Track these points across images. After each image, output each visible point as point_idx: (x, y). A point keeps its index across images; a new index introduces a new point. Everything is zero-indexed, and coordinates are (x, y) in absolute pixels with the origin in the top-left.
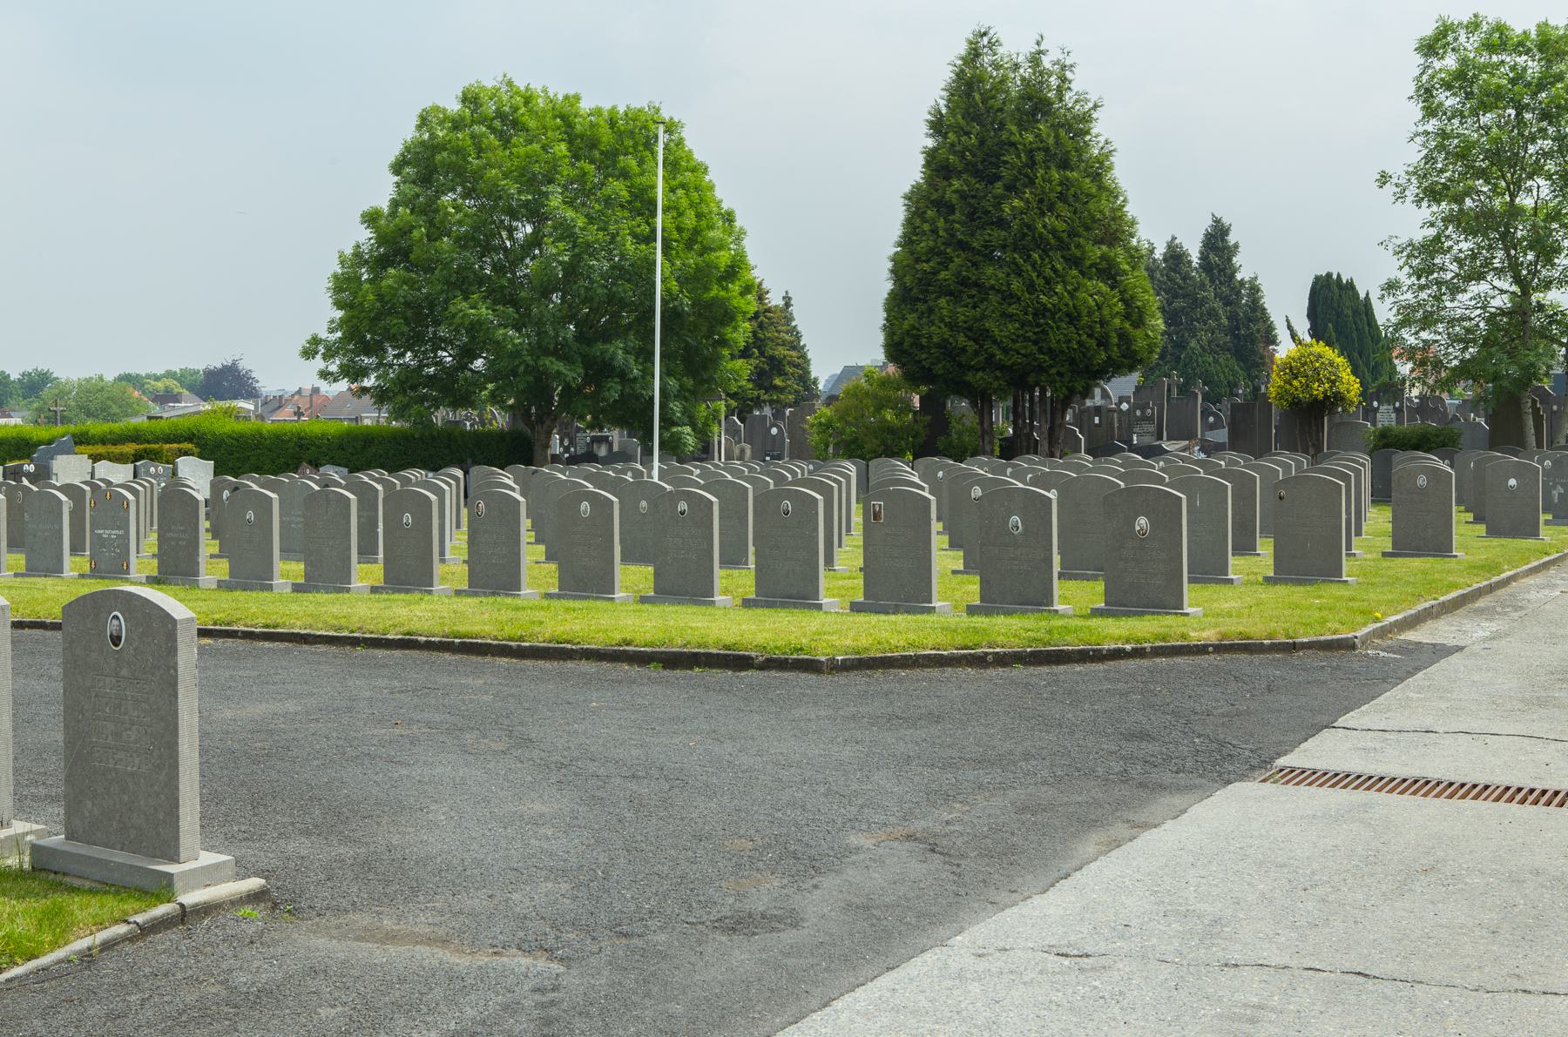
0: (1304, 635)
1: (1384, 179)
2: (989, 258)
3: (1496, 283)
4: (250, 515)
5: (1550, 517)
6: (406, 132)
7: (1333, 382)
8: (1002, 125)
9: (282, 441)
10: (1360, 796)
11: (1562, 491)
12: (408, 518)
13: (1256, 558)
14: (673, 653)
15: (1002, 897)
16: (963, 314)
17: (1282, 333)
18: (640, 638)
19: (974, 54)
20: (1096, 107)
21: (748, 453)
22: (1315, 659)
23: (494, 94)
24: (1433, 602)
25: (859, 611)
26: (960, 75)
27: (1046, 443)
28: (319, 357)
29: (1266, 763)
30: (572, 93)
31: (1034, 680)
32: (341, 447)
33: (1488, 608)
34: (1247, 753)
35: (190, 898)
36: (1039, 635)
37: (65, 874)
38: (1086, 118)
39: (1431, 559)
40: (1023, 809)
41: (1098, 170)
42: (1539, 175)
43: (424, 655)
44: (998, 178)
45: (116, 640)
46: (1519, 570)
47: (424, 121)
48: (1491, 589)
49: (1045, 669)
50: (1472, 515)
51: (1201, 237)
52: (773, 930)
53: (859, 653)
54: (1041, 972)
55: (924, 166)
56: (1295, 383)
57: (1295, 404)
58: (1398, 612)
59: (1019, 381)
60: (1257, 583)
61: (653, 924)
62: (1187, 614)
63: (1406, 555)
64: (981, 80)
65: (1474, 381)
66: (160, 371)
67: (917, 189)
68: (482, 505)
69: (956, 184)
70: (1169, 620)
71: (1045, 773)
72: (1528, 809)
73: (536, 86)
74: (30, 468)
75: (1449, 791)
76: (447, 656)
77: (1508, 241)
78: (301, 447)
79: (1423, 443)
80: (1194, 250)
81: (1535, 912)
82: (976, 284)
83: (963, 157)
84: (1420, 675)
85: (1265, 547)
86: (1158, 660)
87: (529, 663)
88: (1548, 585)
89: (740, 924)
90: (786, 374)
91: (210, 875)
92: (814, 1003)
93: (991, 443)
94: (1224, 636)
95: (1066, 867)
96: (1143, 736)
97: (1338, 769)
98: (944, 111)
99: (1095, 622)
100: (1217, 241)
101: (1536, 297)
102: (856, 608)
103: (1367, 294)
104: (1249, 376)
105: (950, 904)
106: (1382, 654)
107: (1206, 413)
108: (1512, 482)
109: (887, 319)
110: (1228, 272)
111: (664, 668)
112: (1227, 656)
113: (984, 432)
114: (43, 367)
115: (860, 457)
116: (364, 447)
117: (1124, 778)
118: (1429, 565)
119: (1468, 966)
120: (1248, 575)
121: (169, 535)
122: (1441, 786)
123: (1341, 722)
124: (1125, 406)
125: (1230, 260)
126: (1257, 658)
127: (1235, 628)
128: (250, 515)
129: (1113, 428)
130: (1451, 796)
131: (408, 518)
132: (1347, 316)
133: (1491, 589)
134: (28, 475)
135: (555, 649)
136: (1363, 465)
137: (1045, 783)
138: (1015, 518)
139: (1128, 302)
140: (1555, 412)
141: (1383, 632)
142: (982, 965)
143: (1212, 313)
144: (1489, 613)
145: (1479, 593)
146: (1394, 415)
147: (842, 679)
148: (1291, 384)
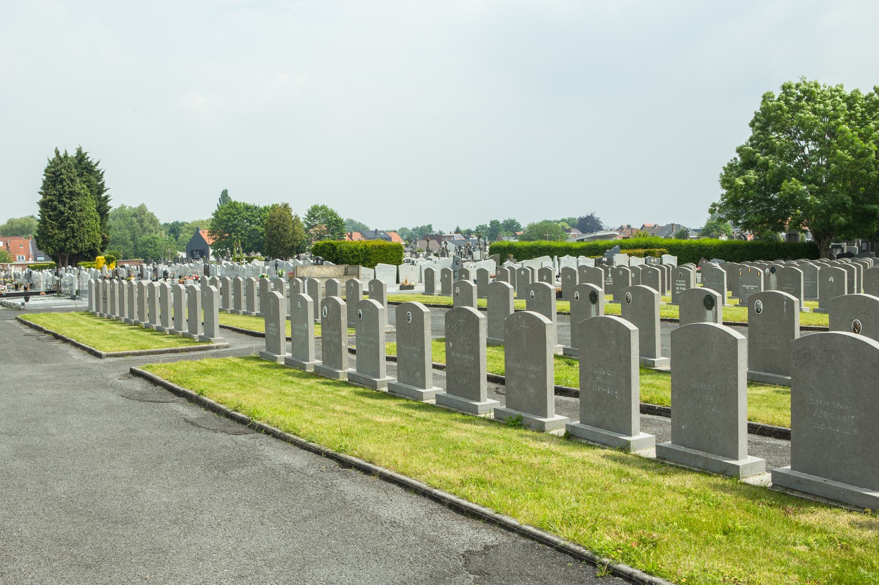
32: (720, 250)
50: (612, 296)
66: (559, 219)
74: (605, 259)
78: (701, 250)
114: (512, 218)
136: (691, 269)
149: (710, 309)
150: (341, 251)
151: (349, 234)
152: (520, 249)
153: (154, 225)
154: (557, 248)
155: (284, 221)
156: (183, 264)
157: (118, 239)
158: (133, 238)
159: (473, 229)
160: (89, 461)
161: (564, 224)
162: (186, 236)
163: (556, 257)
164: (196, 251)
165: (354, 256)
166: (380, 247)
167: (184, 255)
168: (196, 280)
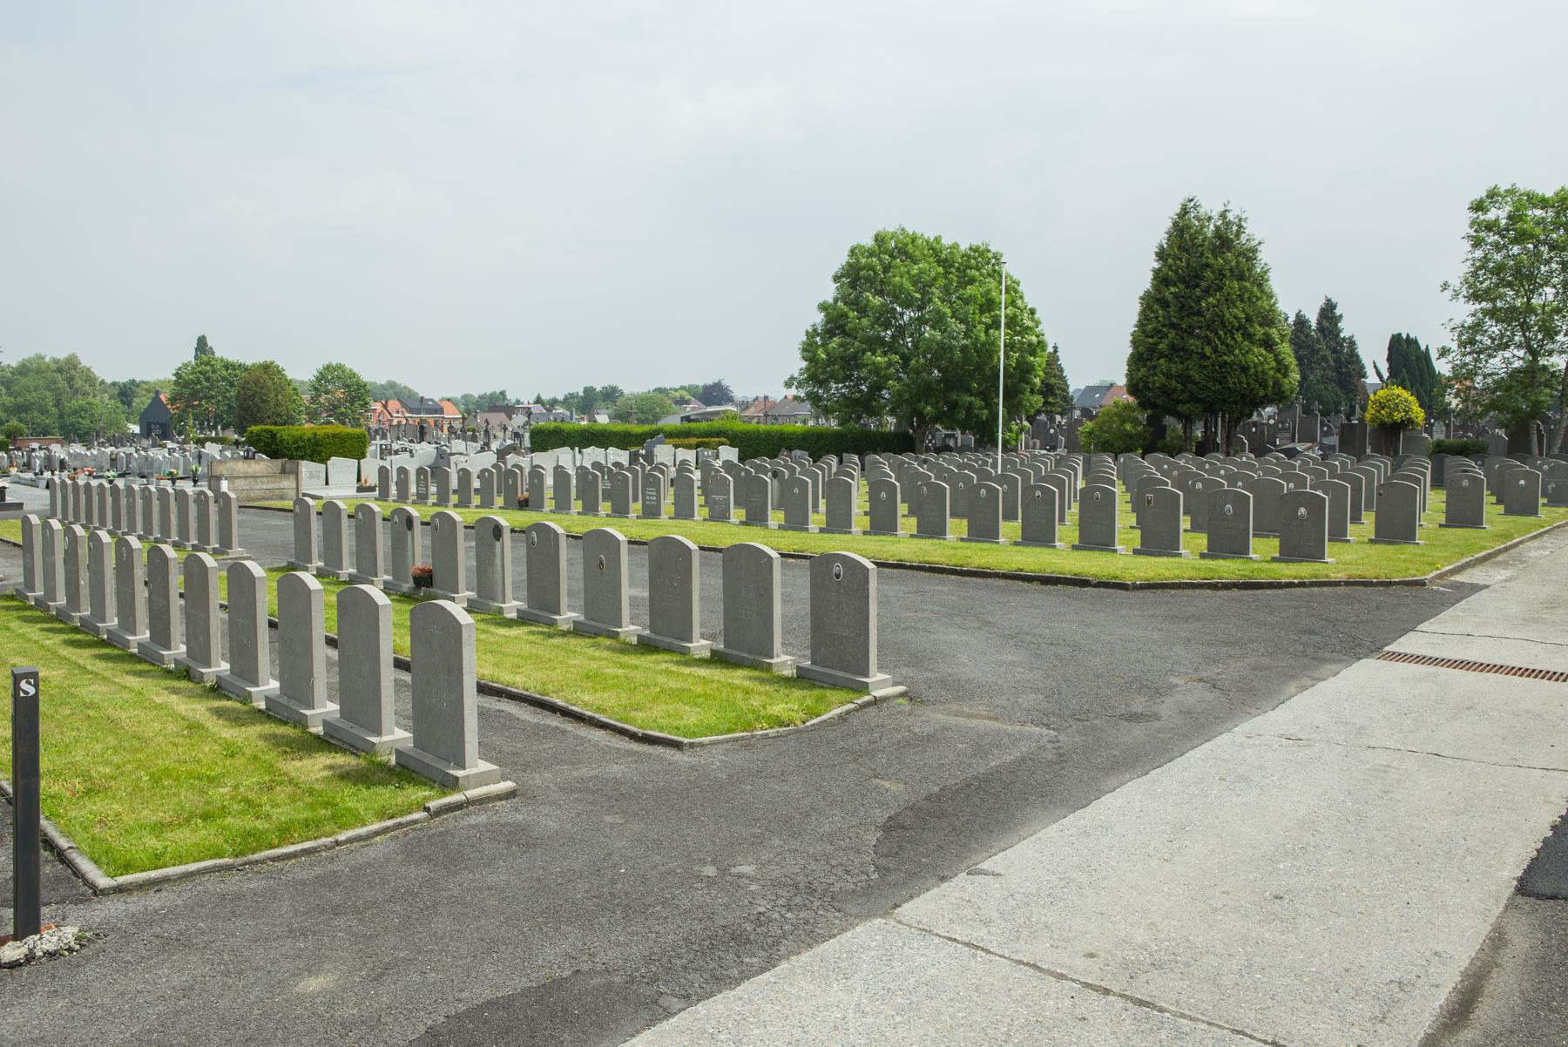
0: (1398, 577)
1: (1445, 286)
2: (1191, 334)
3: (1515, 352)
4: (796, 490)
5: (1545, 501)
6: (841, 259)
7: (1407, 412)
8: (1202, 254)
9: (771, 436)
10: (1432, 669)
11: (1554, 486)
12: (883, 495)
13: (1361, 526)
14: (1047, 577)
15: (1253, 711)
16: (1175, 368)
17: (1370, 371)
18: (1026, 567)
19: (1185, 211)
20: (1260, 243)
21: (1038, 445)
22: (1404, 591)
23: (894, 235)
24: (1471, 558)
25: (1140, 554)
26: (1175, 224)
27: (1225, 446)
28: (794, 387)
29: (1379, 649)
30: (938, 235)
31: (1245, 598)
33: (1504, 561)
34: (1368, 643)
35: (879, 693)
36: (1245, 573)
37: (814, 680)
38: (1254, 250)
39: (1470, 530)
40: (1255, 669)
41: (1260, 282)
42: (1547, 285)
43: (910, 572)
44: (1197, 286)
45: (838, 576)
46: (1524, 537)
47: (853, 252)
48: (1506, 549)
49: (1250, 592)
51: (1318, 310)
52: (1148, 721)
53: (1148, 580)
54: (1280, 746)
55: (1152, 279)
56: (1383, 412)
57: (1383, 425)
58: (1450, 564)
59: (1211, 409)
60: (1364, 543)
61: (1092, 716)
62: (1327, 563)
63: (1454, 527)
64: (1189, 228)
65: (1499, 412)
66: (677, 387)
67: (1147, 293)
68: (925, 489)
69: (1172, 289)
70: (1317, 566)
71: (1262, 650)
72: (1524, 679)
73: (919, 232)
74: (643, 452)
75: (1481, 668)
76: (923, 573)
77: (1525, 327)
78: (781, 438)
79: (1464, 451)
80: (1313, 319)
81: (1526, 731)
82: (1183, 349)
83: (1177, 272)
84: (1463, 602)
85: (1369, 519)
86: (1313, 589)
87: (967, 579)
88: (1542, 548)
89: (1132, 717)
90: (1056, 395)
91: (882, 685)
92: (1177, 754)
93: (1191, 444)
94: (1350, 577)
95: (1282, 698)
96: (1311, 632)
97: (1419, 654)
98: (1165, 246)
99: (1275, 566)
100: (1329, 313)
101: (1542, 361)
102: (1136, 552)
103: (1427, 346)
104: (1348, 398)
105: (1228, 713)
106: (1441, 589)
107: (1323, 424)
108: (1522, 482)
109: (1128, 370)
110: (1335, 333)
111: (1042, 584)
112: (1352, 588)
113: (1186, 437)
114: (613, 384)
115: (1111, 452)
116: (817, 441)
117: (1304, 654)
118: (1468, 534)
119: (1490, 753)
120: (1358, 537)
122: (1477, 665)
123: (1419, 628)
124: (1272, 422)
125: (1337, 325)
126: (1369, 590)
127: (1357, 572)
128: (796, 490)
129: (1264, 435)
130: (1481, 671)
131: (883, 495)
132: (1412, 360)
133: (1506, 549)
134: (642, 456)
135: (981, 572)
137: (1263, 655)
138: (1229, 506)
139: (1279, 361)
140: (1552, 430)
141: (1441, 576)
142: (1251, 741)
143: (1324, 358)
144: (1505, 564)
145: (1499, 552)
146: (1444, 428)
147: (1140, 594)
148: (1380, 413)
149: (498, 540)
150: (281, 441)
151: (384, 402)
152: (568, 433)
153: (90, 386)
154: (614, 433)
155: (262, 388)
156: (117, 448)
157: (34, 404)
158: (57, 404)
159: (561, 398)
160: (1113, 702)
161: (684, 393)
162: (142, 402)
163: (577, 449)
164: (155, 424)
165: (299, 447)
166: (334, 436)
167: (136, 429)
168: (90, 475)
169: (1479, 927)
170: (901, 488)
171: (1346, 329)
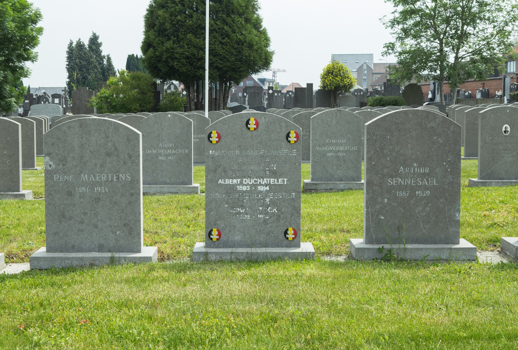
100: (94, 41)
121: (392, 182)
143: (95, 67)
169: (471, 4)
170: (143, 135)
171: (105, 51)
